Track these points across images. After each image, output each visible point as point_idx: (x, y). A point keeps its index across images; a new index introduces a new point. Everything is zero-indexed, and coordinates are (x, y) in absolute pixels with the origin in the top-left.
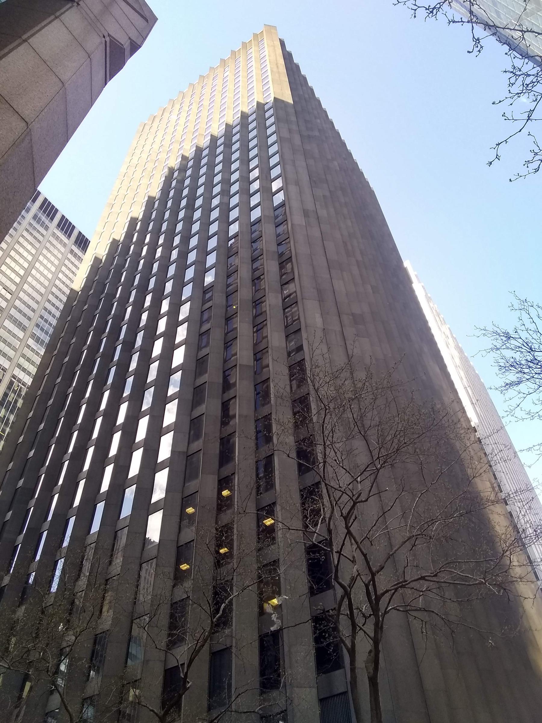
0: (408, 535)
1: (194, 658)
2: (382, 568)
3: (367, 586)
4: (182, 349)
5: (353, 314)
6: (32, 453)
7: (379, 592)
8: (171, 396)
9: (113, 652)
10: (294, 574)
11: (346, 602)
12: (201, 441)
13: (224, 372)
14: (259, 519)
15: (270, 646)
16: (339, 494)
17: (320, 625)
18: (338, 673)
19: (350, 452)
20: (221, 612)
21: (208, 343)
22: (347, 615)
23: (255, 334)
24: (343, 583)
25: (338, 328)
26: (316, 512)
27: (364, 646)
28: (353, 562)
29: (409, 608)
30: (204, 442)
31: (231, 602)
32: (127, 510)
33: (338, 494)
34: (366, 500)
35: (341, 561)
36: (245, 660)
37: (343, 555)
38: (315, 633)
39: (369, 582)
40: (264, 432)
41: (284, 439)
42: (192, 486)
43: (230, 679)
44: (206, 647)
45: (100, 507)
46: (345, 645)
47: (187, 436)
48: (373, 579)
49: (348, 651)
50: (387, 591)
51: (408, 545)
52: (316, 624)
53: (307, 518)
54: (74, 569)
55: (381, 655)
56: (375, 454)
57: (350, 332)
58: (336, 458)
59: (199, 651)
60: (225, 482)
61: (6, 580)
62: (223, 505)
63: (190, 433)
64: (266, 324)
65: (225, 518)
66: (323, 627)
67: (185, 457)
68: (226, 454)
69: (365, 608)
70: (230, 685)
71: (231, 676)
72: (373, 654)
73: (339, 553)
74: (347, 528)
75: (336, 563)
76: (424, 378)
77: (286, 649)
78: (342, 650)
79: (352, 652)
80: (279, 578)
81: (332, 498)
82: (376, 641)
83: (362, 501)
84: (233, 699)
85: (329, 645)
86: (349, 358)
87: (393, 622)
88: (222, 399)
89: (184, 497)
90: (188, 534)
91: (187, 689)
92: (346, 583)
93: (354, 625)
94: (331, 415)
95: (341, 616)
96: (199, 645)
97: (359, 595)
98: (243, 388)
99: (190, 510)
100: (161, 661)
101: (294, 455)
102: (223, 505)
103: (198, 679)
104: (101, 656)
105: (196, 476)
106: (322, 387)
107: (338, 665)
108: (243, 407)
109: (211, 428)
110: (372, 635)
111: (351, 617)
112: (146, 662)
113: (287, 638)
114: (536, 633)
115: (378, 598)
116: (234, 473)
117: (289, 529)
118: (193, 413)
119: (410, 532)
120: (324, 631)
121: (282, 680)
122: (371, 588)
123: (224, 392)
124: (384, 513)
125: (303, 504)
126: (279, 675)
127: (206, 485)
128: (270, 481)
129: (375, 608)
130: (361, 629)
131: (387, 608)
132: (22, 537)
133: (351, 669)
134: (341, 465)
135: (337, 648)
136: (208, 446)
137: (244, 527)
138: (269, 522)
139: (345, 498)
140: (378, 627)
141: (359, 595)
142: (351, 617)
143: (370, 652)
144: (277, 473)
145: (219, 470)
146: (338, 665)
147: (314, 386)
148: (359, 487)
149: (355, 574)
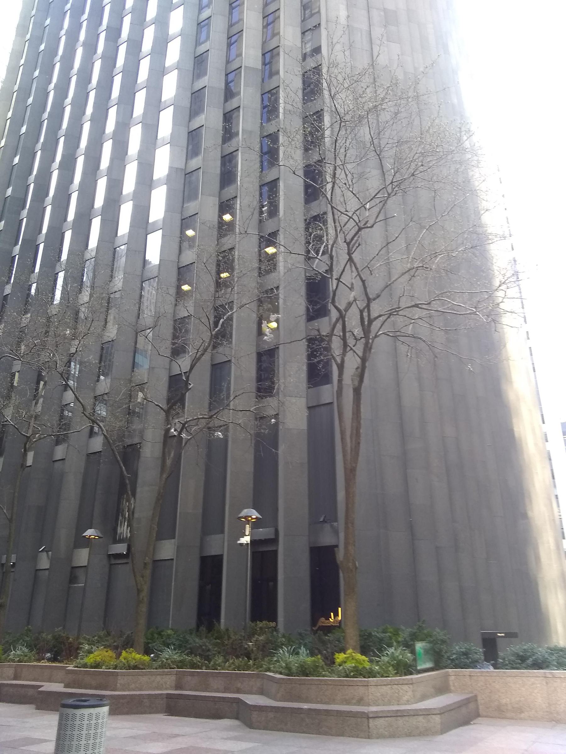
0: (409, 266)
1: (195, 364)
2: (378, 296)
3: (361, 312)
4: (178, 41)
5: (385, 10)
6: (16, 160)
7: (372, 317)
8: (165, 101)
9: (120, 360)
10: (293, 300)
11: (339, 326)
12: (200, 158)
13: (227, 75)
14: (261, 249)
15: (266, 359)
16: (344, 218)
17: (313, 344)
18: (327, 387)
19: (361, 176)
20: (219, 326)
21: (208, 37)
22: (340, 336)
23: (265, 30)
24: (339, 307)
25: (364, 27)
26: (319, 239)
27: (352, 363)
28: (350, 289)
29: (398, 334)
30: (204, 160)
31: (230, 319)
32: (124, 228)
33: (344, 218)
34: (372, 227)
35: (339, 288)
36: (243, 371)
37: (341, 282)
38: (308, 351)
39: (364, 308)
40: (269, 154)
41: (291, 156)
42: (192, 207)
43: (229, 383)
44: (207, 357)
45: (96, 223)
46: (335, 361)
47: (185, 151)
48: (368, 306)
49: (338, 365)
50: (380, 316)
51: (407, 277)
52: (309, 343)
53: (310, 243)
54: (75, 281)
55: (367, 371)
56: (389, 179)
57: (377, 31)
58: (346, 182)
59: (199, 359)
60: (225, 206)
61: (8, 290)
62: (224, 229)
63: (187, 148)
64: (279, 17)
65: (228, 242)
66: (316, 348)
67: (183, 176)
68: (227, 177)
69: (358, 332)
70: (229, 388)
71: (230, 381)
72: (359, 370)
73: (338, 280)
74: (349, 254)
75: (335, 288)
76: (455, 101)
77: (281, 361)
78: (331, 366)
79: (341, 367)
80: (278, 304)
81: (337, 224)
82: (364, 360)
83: (368, 227)
84: (232, 398)
85: (319, 362)
86: (373, 64)
87: (381, 345)
88: (224, 109)
89: (183, 218)
90: (189, 257)
91: (188, 390)
92: (342, 307)
93: (345, 345)
94: (346, 130)
95: (334, 337)
96: (199, 353)
97: (353, 320)
98: (248, 97)
99: (190, 233)
100: (165, 369)
101: (301, 173)
102: (224, 229)
103: (200, 384)
104: (110, 361)
105: (196, 197)
106: (337, 100)
107: (326, 379)
108: (248, 122)
109: (211, 140)
110: (361, 354)
111: (344, 339)
112: (151, 369)
113: (282, 353)
114: (511, 363)
115: (371, 322)
116: (236, 197)
117: (291, 253)
118: (191, 123)
119: (412, 263)
120: (316, 351)
121: (276, 387)
122: (365, 314)
123: (226, 100)
124: (388, 243)
125: (307, 229)
126: (273, 383)
127: (206, 207)
128: (273, 202)
129: (366, 331)
130: (351, 349)
131: (377, 332)
132: (17, 249)
133: (338, 380)
134: (351, 189)
135: (327, 364)
136: (209, 162)
137: (245, 248)
138: (271, 250)
139: (351, 223)
140: (368, 348)
141: (353, 320)
142: (344, 339)
143: (357, 368)
144: (281, 193)
145: (220, 193)
146: (326, 379)
147: (330, 91)
148: (367, 214)
149: (351, 299)
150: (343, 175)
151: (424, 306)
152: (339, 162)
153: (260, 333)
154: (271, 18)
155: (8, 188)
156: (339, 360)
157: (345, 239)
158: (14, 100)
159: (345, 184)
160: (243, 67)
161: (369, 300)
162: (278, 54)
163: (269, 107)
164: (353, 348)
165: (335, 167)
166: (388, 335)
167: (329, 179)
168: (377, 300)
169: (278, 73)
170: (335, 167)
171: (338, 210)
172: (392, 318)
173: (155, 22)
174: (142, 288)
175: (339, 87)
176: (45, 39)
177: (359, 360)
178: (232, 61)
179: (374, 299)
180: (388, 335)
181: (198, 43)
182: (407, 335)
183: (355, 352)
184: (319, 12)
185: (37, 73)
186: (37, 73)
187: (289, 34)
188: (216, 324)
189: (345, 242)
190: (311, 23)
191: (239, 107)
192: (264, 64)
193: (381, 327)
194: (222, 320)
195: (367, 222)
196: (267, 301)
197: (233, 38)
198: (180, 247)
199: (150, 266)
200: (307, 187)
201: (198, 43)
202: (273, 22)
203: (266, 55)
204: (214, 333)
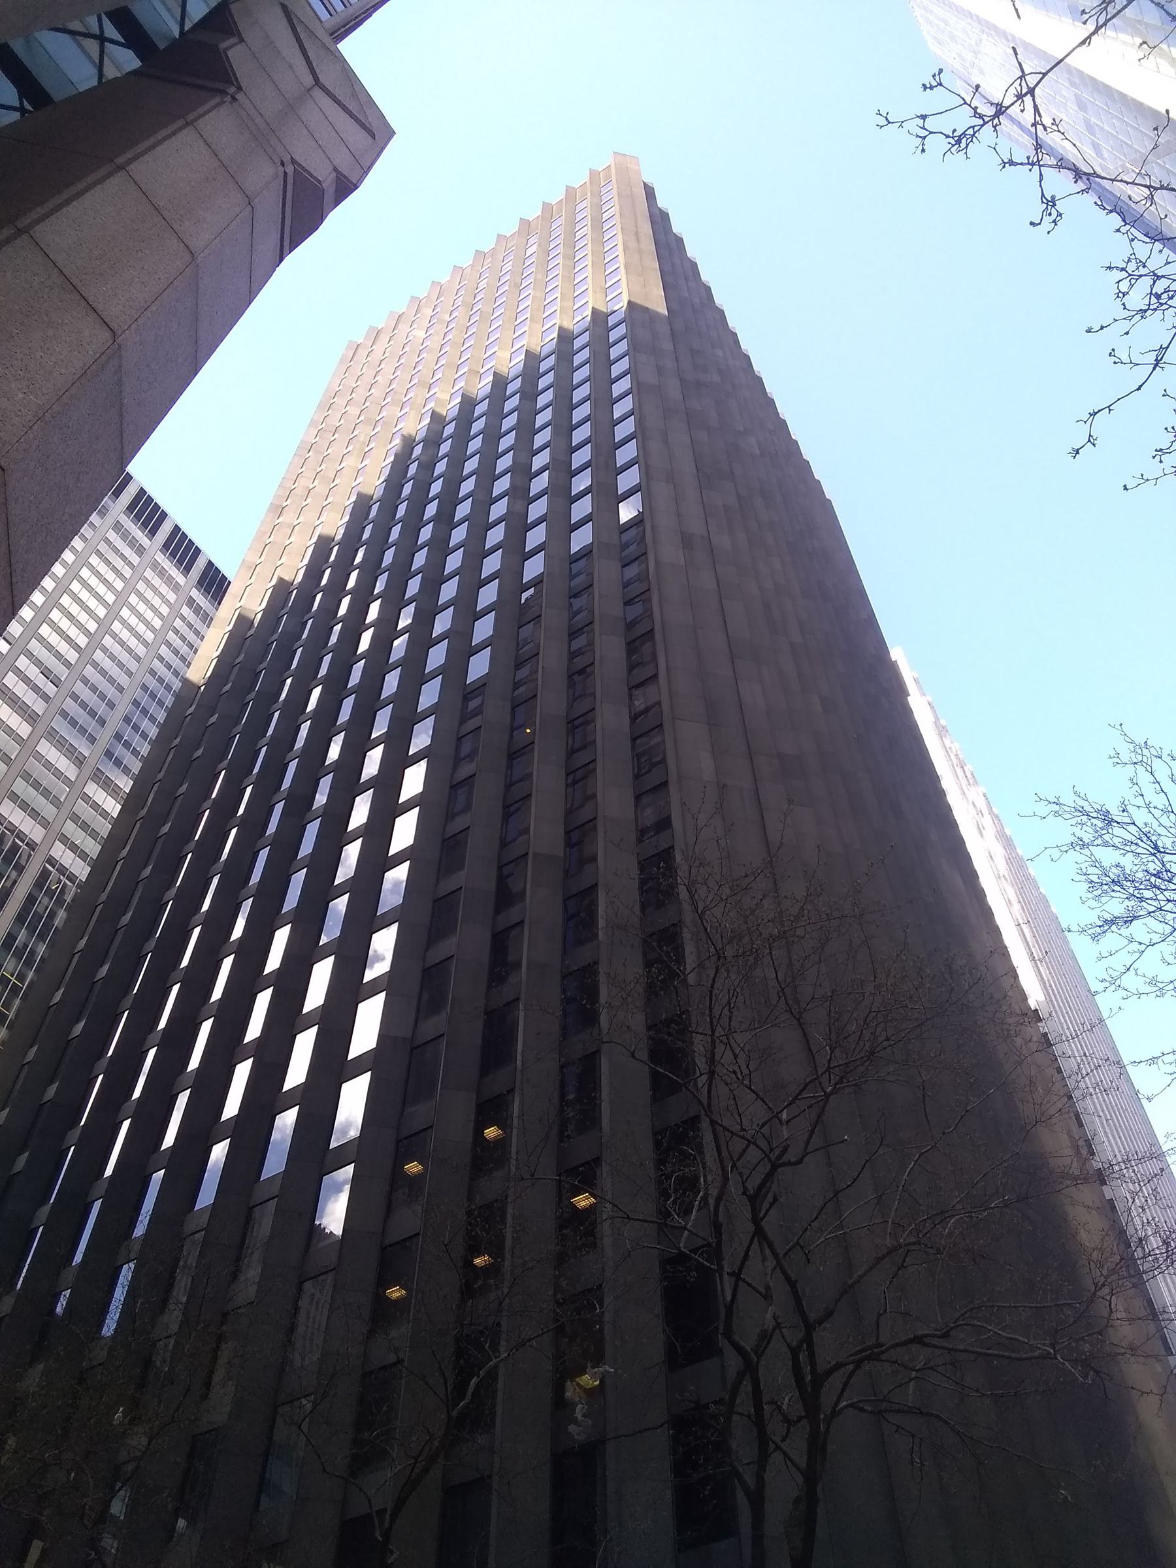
0: (888, 1242)
2: (829, 1314)
3: (794, 1352)
6: (79, 1028)
7: (822, 1367)
11: (747, 1386)
15: (576, 1474)
16: (738, 1145)
21: (468, 807)
22: (749, 1416)
23: (570, 790)
24: (742, 1343)
26: (690, 1184)
27: (782, 1485)
29: (884, 1405)
31: (493, 1375)
34: (800, 1161)
37: (744, 1281)
41: (623, 1017)
48: (808, 1339)
50: (839, 1366)
58: (736, 1068)
60: (491, 1108)
63: (419, 999)
66: (694, 1438)
69: (789, 1401)
73: (737, 1275)
74: (756, 1221)
75: (729, 1298)
79: (757, 1500)
81: (725, 1154)
82: (811, 1478)
83: (789, 1164)
90: (407, 1220)
93: (763, 1440)
94: (728, 971)
95: (736, 1418)
97: (776, 1371)
98: (540, 903)
101: (643, 1054)
102: (486, 1158)
110: (803, 1463)
111: (759, 1421)
115: (819, 1380)
122: (803, 1357)
125: (660, 1162)
130: (778, 1448)
131: (837, 1404)
138: (583, 1201)
139: (753, 1154)
140: (817, 1446)
141: (776, 1371)
142: (759, 1421)
143: (797, 1501)
147: (695, 905)
149: (769, 1323)
150: (729, 1056)
151: (935, 1341)
152: (719, 1032)
153: (560, 1403)
154: (579, 774)
155: (52, 1082)
156: (750, 1479)
157: (745, 1187)
158: (95, 918)
159: (734, 1072)
160: (530, 856)
161: (809, 1328)
162: (595, 828)
163: (579, 913)
164: (784, 1446)
165: (713, 1042)
166: (862, 1410)
167: (701, 1063)
168: (827, 1325)
169: (594, 859)
170: (713, 1042)
171: (724, 1128)
172: (867, 1366)
173: (350, 886)
174: (300, 1289)
175: (710, 899)
176: (172, 816)
177: (800, 1479)
178: (511, 842)
179: (820, 1322)
180: (862, 1410)
181: (450, 816)
182: (906, 1408)
183: (785, 1454)
184: (664, 761)
185: (147, 872)
186: (147, 872)
187: (613, 798)
188: (460, 1389)
189: (744, 1193)
190: (642, 673)
191: (523, 921)
192: (569, 844)
193: (843, 1390)
194: (474, 1380)
195: (785, 1149)
196: (577, 1333)
197: (513, 805)
198: (390, 1200)
199: (321, 1245)
200: (655, 1077)
201: (450, 816)
202: (585, 778)
203: (572, 834)
204: (454, 1413)
